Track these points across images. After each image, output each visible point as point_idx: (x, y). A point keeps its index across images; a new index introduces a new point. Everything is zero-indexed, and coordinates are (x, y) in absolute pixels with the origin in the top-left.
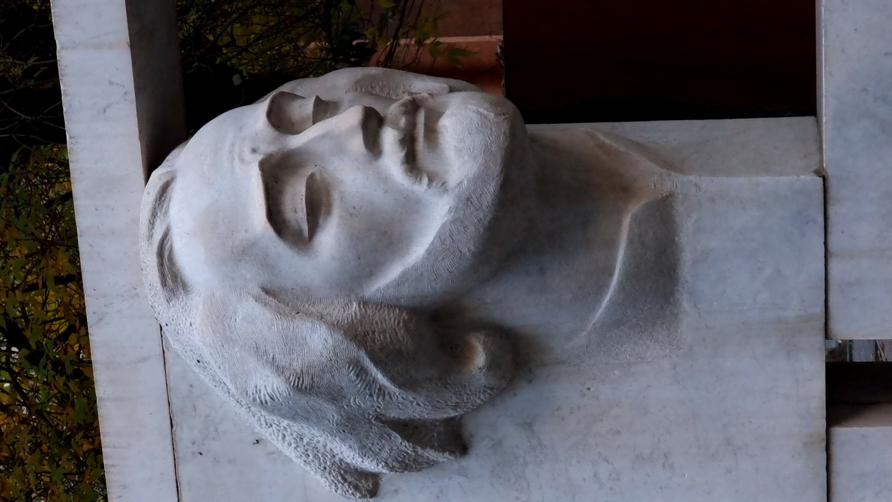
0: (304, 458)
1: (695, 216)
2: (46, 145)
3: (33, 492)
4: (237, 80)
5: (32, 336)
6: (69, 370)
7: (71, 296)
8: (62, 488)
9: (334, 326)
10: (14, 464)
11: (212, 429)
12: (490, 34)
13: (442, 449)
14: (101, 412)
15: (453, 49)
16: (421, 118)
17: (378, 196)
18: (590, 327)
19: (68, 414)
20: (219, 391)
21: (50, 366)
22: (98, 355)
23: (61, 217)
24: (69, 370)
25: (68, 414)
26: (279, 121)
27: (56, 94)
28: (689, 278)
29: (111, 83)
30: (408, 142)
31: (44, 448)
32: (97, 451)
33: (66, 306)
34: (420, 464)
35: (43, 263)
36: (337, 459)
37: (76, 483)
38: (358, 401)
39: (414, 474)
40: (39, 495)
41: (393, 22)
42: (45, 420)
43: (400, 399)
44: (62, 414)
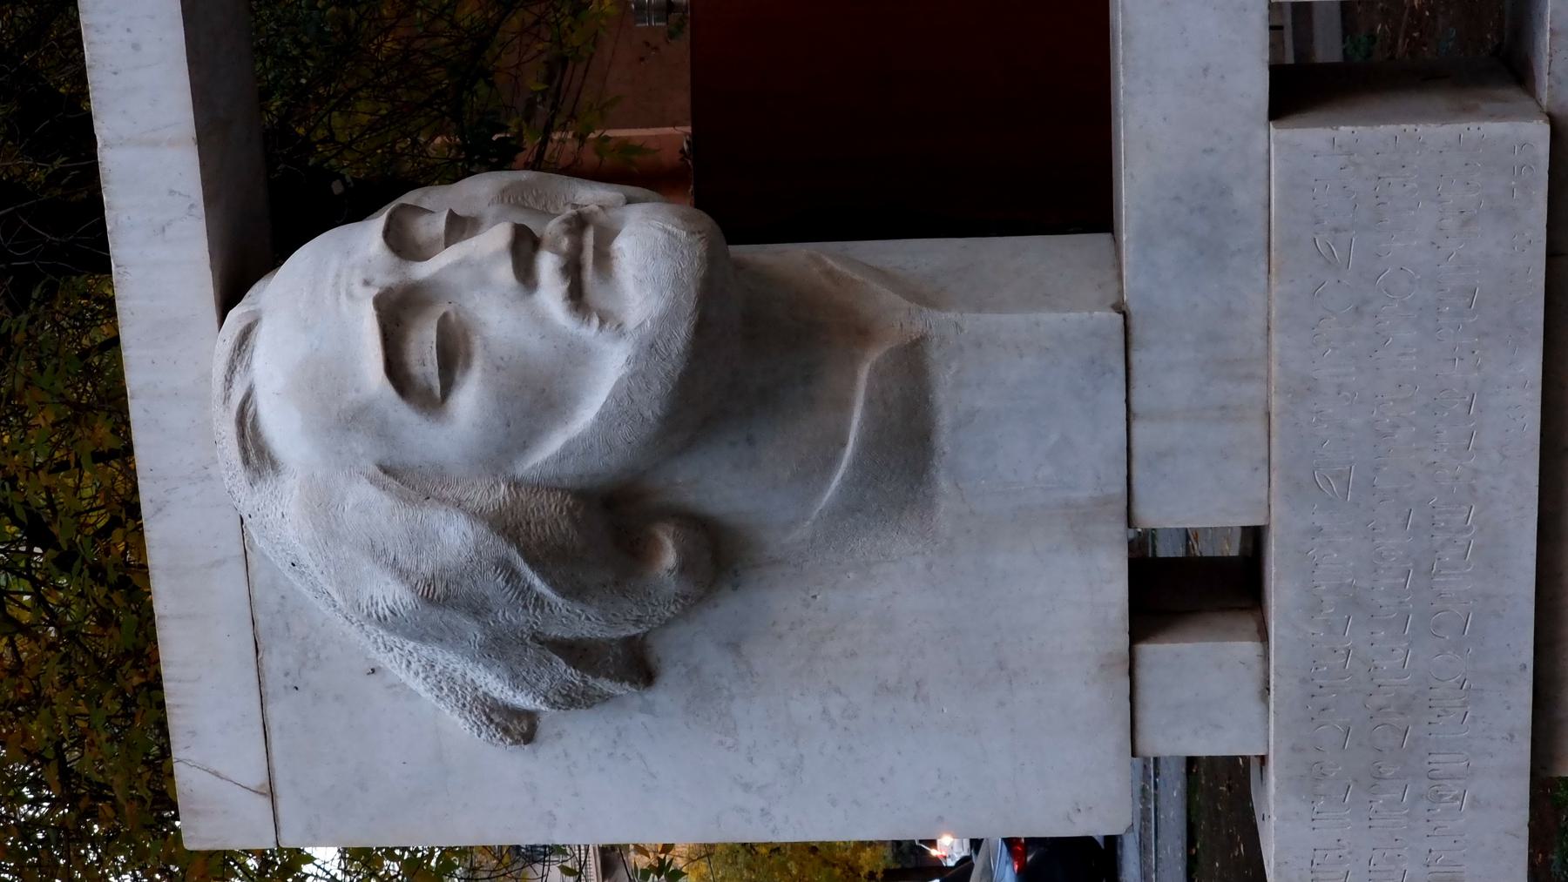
0: (436, 691)
1: (954, 366)
2: (79, 275)
3: (64, 740)
4: (337, 188)
5: (62, 532)
6: (112, 577)
7: (114, 480)
8: (104, 736)
9: (476, 515)
10: (39, 704)
11: (311, 655)
12: (674, 125)
13: (620, 678)
14: (161, 634)
15: (625, 146)
16: (589, 238)
17: (534, 343)
18: (815, 514)
19: (111, 636)
20: (321, 604)
21: (86, 573)
22: (157, 557)
23: (101, 371)
24: (112, 577)
25: (111, 636)
26: (401, 243)
27: (94, 207)
28: (947, 449)
29: (172, 192)
30: (572, 270)
31: (80, 681)
32: (154, 684)
33: (109, 492)
34: (591, 698)
35: (78, 433)
36: (480, 693)
37: (122, 729)
38: (510, 616)
39: (584, 712)
40: (73, 745)
41: (543, 110)
42: (81, 645)
43: (564, 611)
44: (102, 636)
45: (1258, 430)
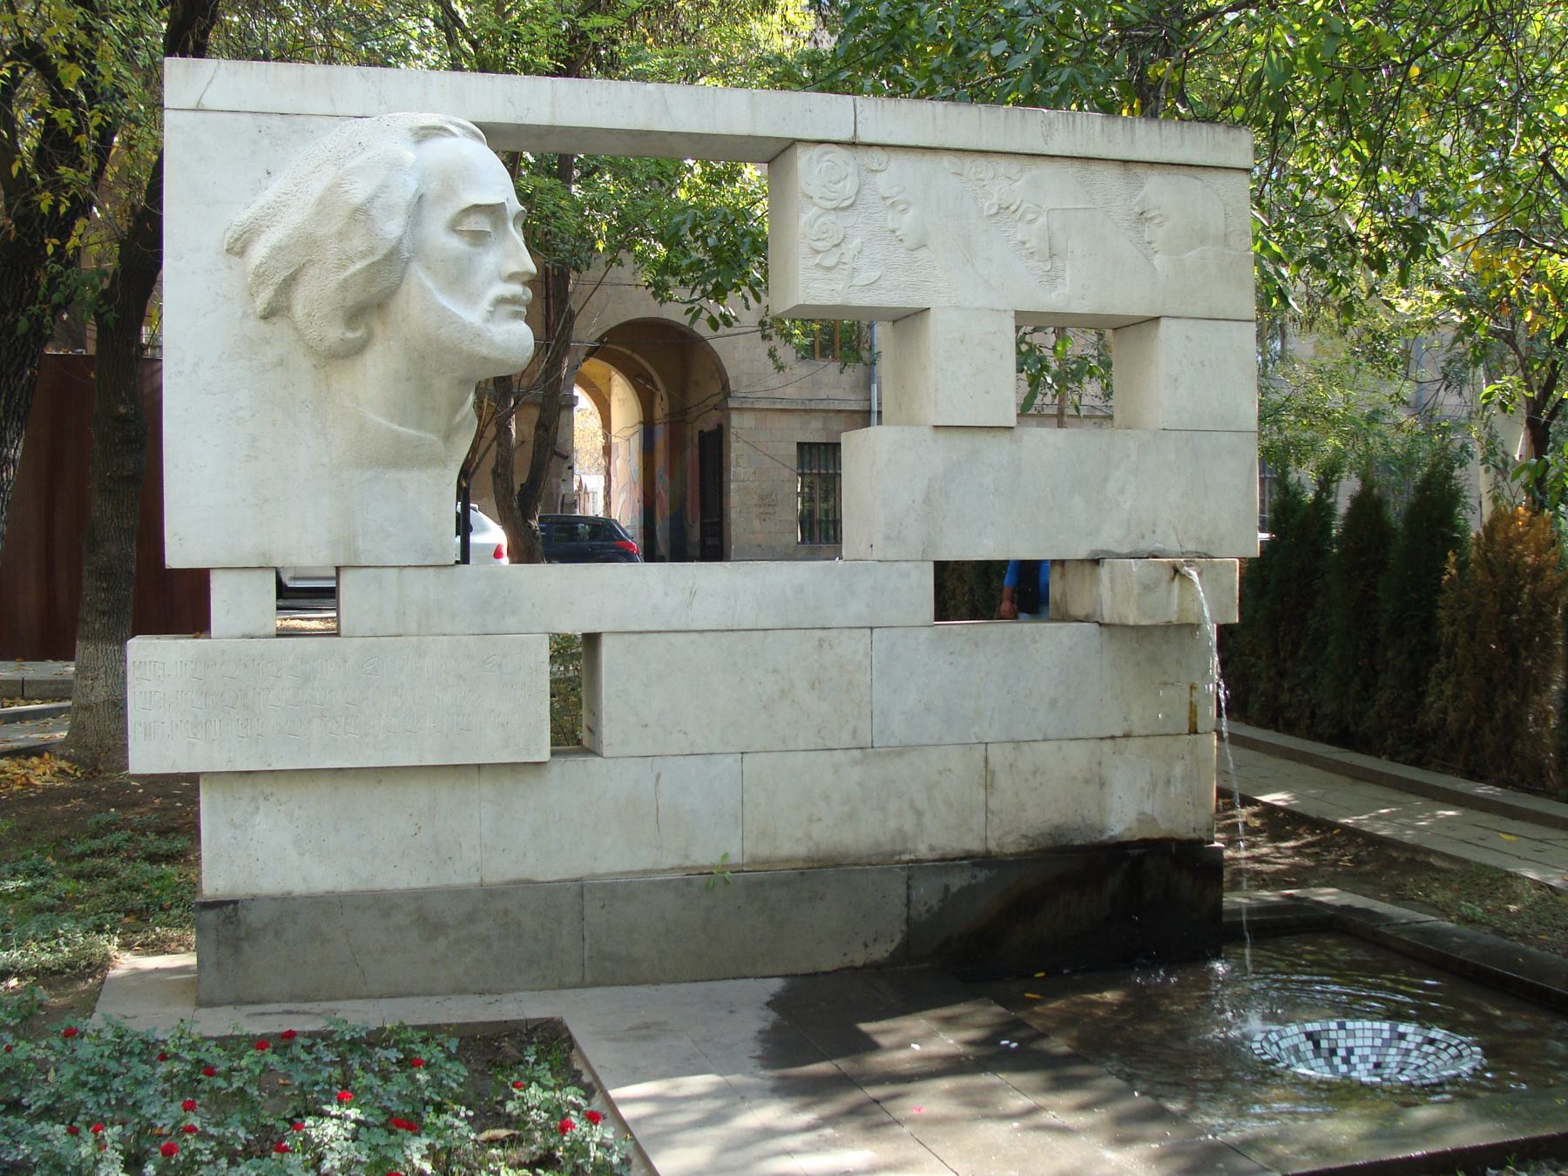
9: (400, 241)
45: (393, 631)
